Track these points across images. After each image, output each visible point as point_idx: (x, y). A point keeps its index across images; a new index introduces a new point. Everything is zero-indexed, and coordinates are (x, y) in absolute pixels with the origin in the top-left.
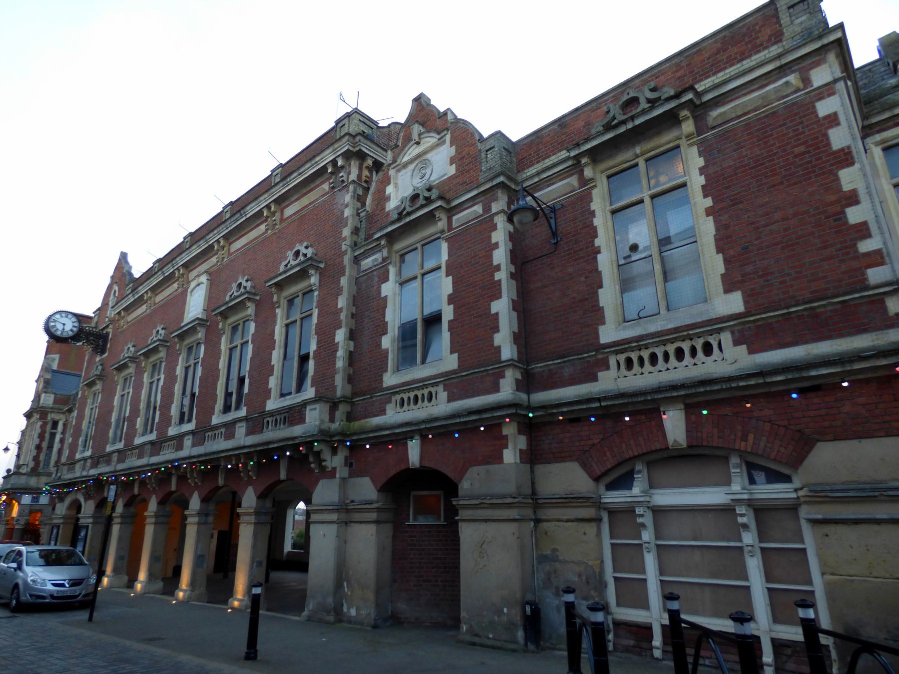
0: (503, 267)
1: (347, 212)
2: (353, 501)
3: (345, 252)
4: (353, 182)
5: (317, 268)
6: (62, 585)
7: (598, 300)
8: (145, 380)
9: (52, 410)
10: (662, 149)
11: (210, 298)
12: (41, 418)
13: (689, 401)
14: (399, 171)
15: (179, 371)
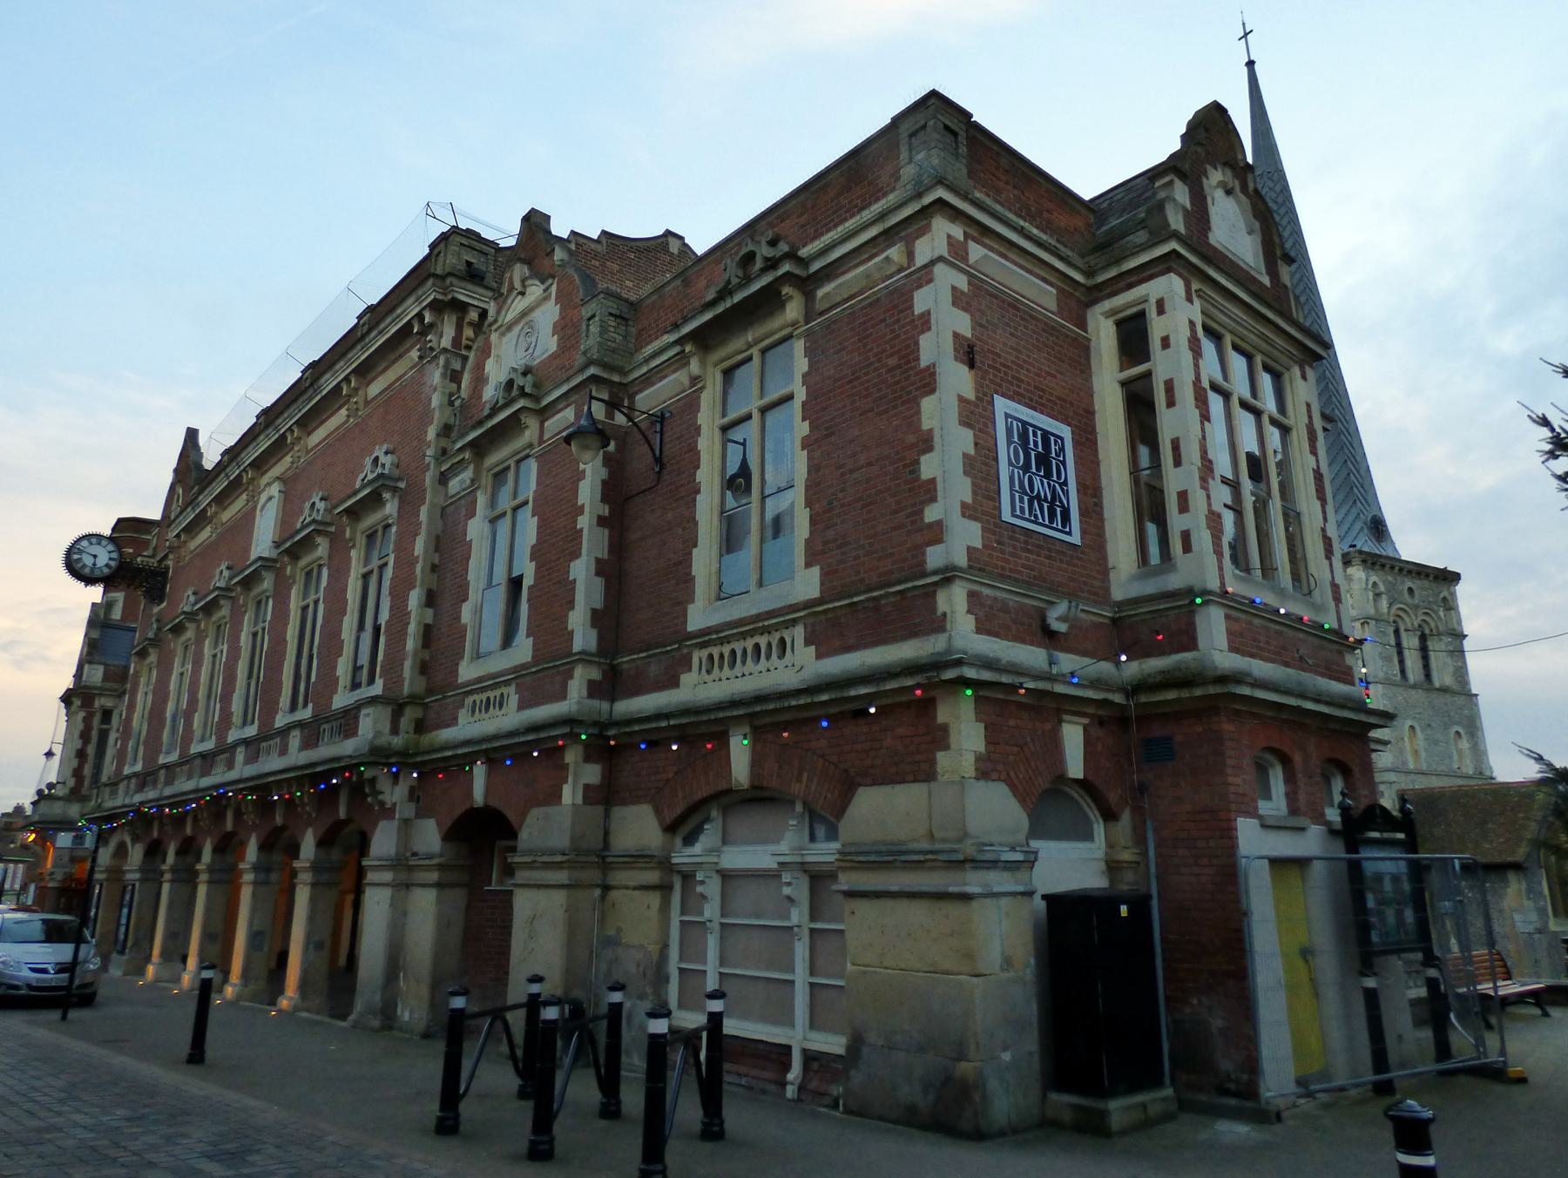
0: (587, 509)
1: (436, 401)
2: (415, 854)
3: (427, 467)
4: (445, 350)
5: (395, 490)
6: (44, 971)
7: (690, 566)
8: (206, 650)
9: (102, 691)
10: (777, 337)
11: (285, 521)
12: (83, 706)
13: (757, 723)
14: (503, 334)
15: (245, 639)
